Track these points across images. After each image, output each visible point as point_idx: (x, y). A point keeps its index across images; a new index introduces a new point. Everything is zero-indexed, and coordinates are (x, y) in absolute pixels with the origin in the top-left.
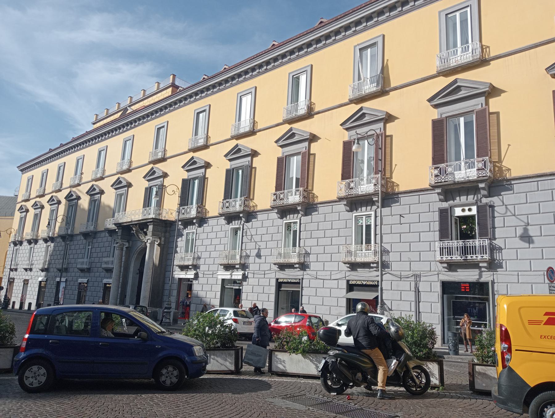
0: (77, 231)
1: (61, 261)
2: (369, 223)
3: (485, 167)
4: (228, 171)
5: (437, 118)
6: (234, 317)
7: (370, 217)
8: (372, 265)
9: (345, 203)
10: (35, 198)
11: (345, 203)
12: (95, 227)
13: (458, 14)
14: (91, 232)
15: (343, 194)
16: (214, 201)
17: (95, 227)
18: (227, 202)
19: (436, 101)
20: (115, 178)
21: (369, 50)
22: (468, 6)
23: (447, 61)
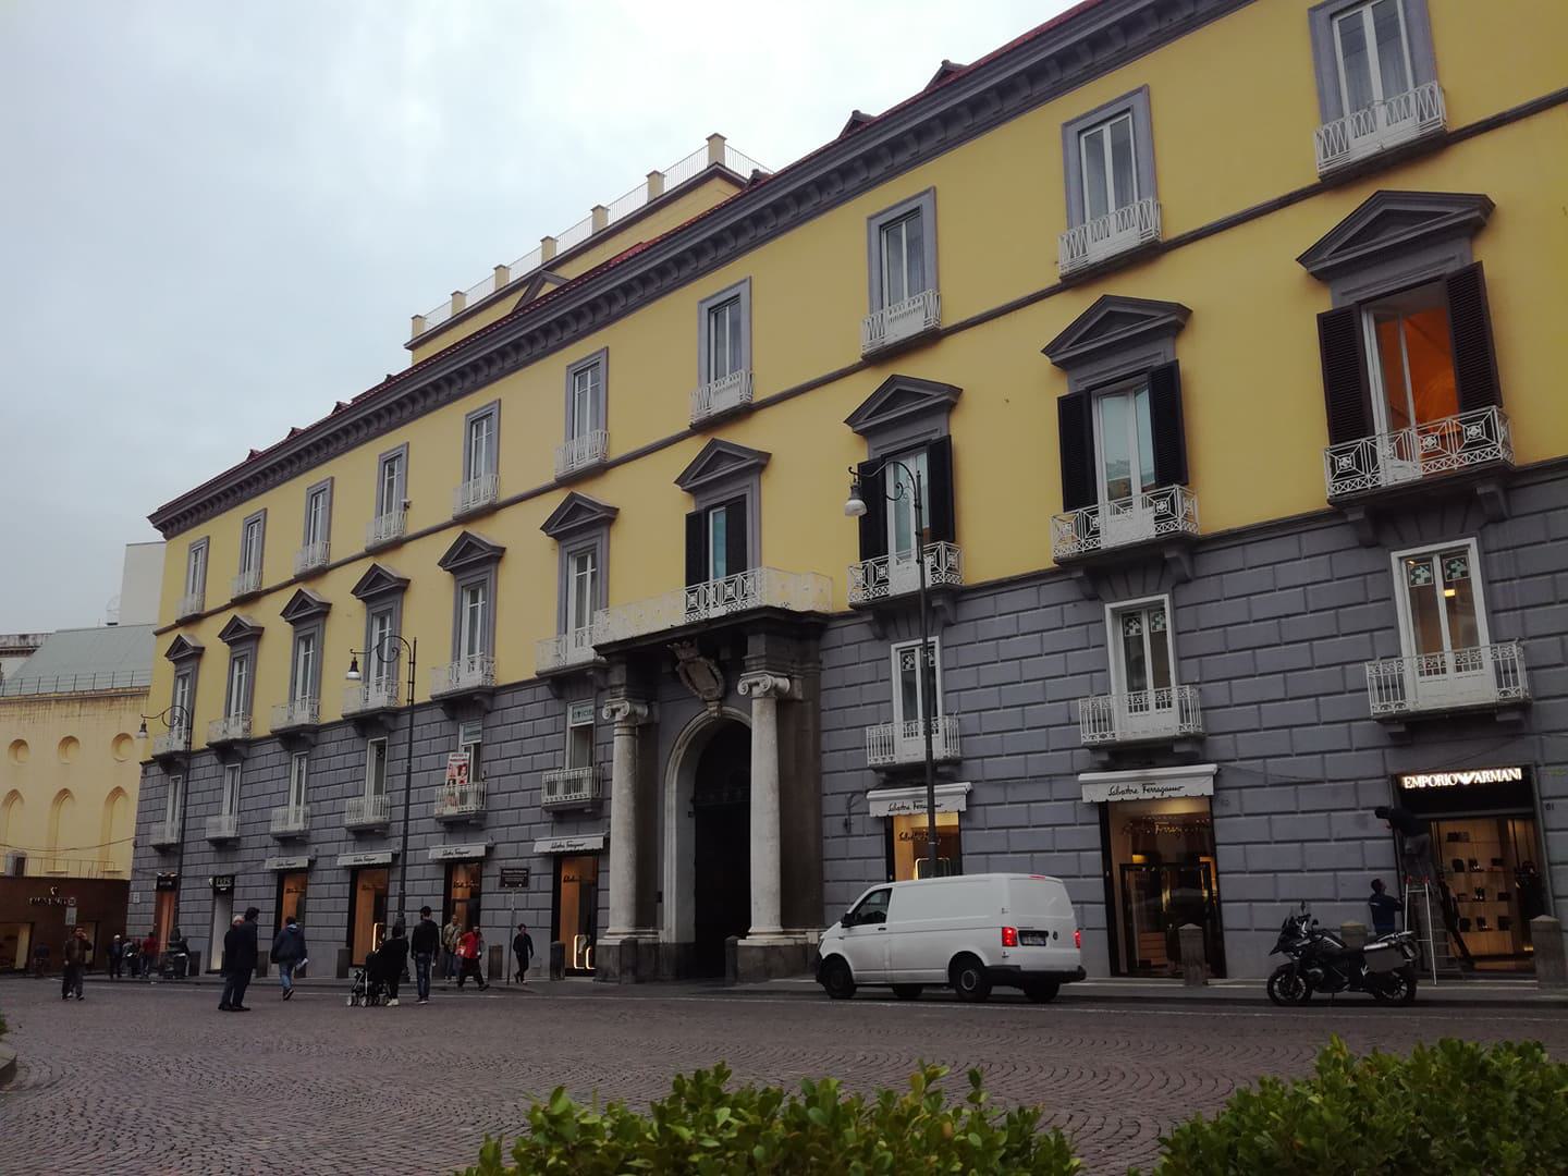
0: (262, 729)
1: (416, 780)
2: (1159, 628)
3: (1489, 435)
4: (1325, 321)
5: (1067, 393)
6: (142, 943)
7: (1465, 552)
8: (1178, 749)
9: (871, 618)
10: (227, 607)
11: (871, 618)
12: (316, 713)
13: (1106, 129)
14: (384, 711)
15: (1070, 549)
16: (1012, 519)
17: (316, 713)
18: (731, 599)
19: (1322, 264)
20: (362, 568)
21: (485, 422)
22: (1128, 110)
23: (1341, 150)
